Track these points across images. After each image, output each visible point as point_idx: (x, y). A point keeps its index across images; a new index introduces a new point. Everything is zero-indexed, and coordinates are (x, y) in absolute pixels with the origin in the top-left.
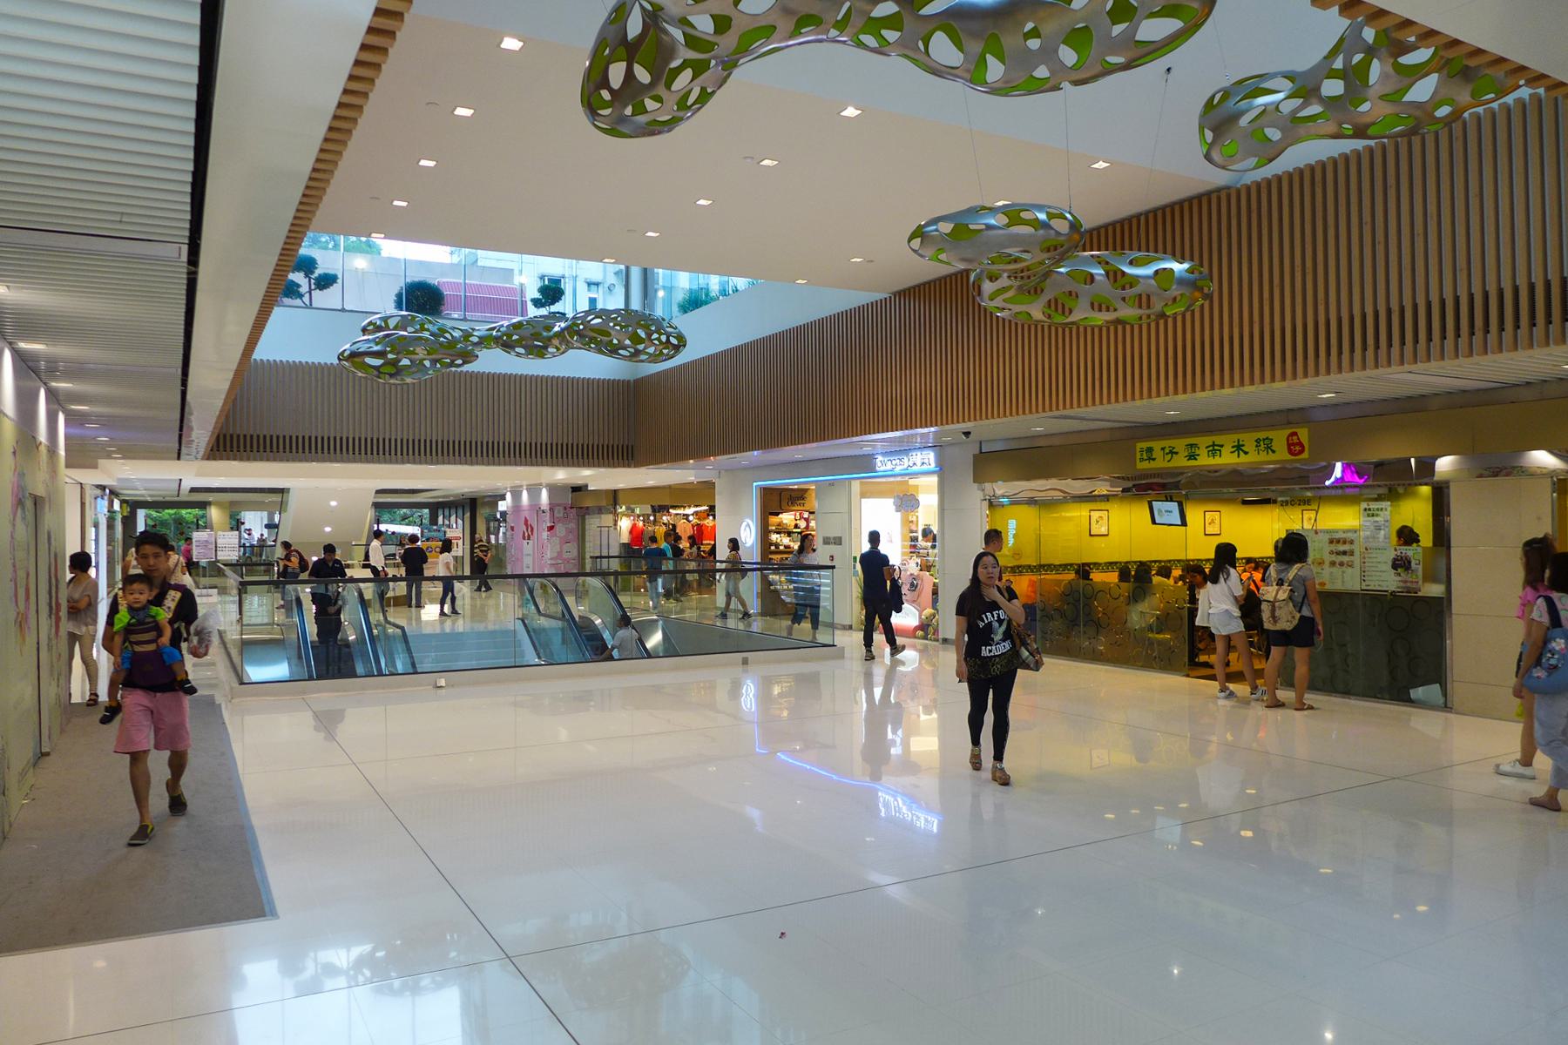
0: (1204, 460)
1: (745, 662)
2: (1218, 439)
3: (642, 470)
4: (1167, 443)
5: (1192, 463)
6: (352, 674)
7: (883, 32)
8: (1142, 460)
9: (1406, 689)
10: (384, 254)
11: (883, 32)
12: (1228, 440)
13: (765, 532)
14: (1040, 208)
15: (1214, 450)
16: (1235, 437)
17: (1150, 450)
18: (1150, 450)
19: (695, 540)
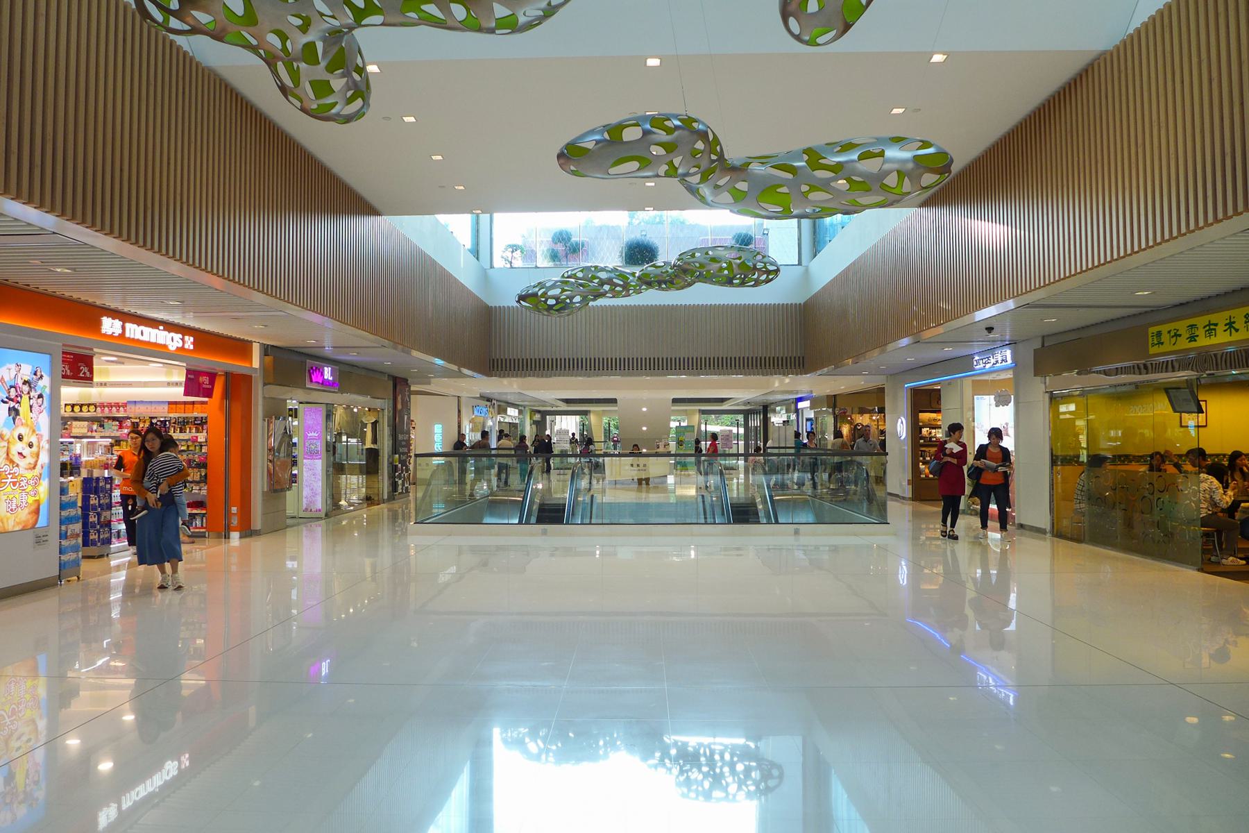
0: (1203, 341)
1: (797, 532)
2: (1213, 318)
3: (505, 381)
4: (1172, 326)
5: (1193, 345)
6: (758, 523)
7: (423, 7)
8: (1153, 345)
9: (482, 518)
10: (986, 441)
11: (423, 7)
12: (1221, 318)
13: (916, 427)
14: (847, 147)
15: (1211, 329)
16: (1226, 314)
17: (1159, 334)
18: (1159, 334)
19: (811, 434)
